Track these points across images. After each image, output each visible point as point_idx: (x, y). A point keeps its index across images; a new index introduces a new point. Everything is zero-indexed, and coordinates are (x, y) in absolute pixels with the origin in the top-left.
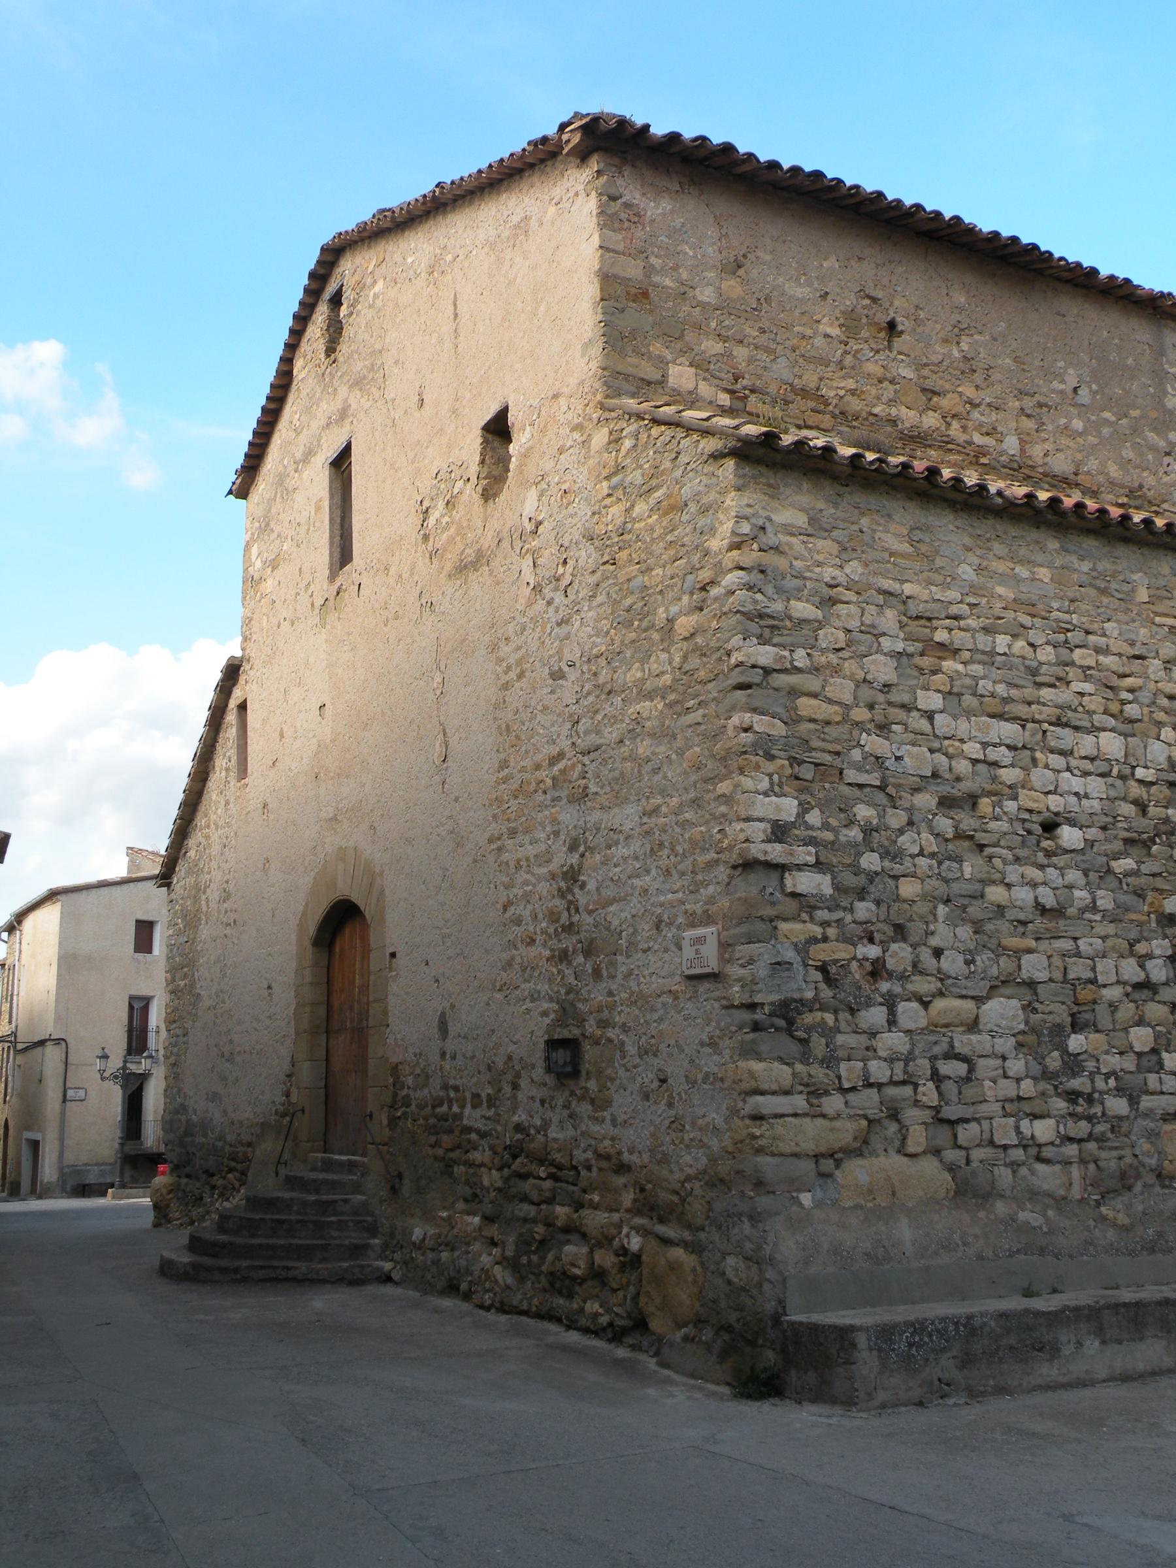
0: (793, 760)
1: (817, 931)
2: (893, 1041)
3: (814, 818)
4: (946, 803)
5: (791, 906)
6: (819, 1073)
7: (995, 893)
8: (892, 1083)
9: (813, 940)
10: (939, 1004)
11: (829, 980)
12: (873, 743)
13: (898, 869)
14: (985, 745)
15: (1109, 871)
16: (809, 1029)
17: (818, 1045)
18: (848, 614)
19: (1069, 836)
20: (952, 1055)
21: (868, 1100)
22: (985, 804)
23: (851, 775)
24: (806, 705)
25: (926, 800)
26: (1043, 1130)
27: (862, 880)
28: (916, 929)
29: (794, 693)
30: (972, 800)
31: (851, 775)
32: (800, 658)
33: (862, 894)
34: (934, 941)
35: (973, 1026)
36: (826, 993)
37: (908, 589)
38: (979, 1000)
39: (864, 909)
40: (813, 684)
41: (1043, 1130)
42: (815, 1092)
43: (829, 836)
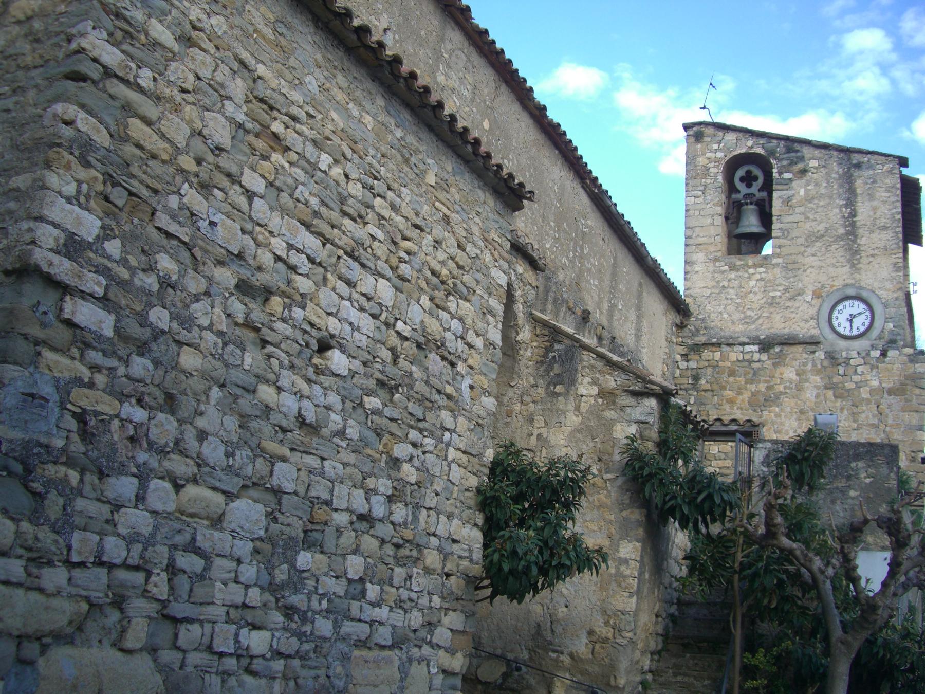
0: (109, 178)
1: (85, 373)
2: (135, 519)
3: (113, 247)
4: (244, 288)
5: (62, 335)
6: (47, 537)
7: (266, 393)
8: (126, 566)
9: (78, 381)
10: (191, 490)
11: (86, 435)
12: (193, 198)
13: (184, 336)
14: (290, 247)
15: (361, 404)
16: (50, 483)
17: (54, 504)
18: (202, 61)
19: (337, 360)
20: (192, 547)
21: (95, 581)
22: (276, 303)
23: (163, 220)
24: (136, 128)
25: (226, 276)
26: (257, 641)
27: (147, 333)
28: (187, 405)
29: (128, 109)
30: (267, 293)
31: (163, 220)
32: (145, 78)
33: (143, 349)
34: (201, 423)
35: (217, 522)
36: (77, 446)
37: (261, 70)
38: (229, 496)
39: (140, 366)
40: (151, 110)
41: (257, 641)
42: (38, 559)
43: (125, 274)
